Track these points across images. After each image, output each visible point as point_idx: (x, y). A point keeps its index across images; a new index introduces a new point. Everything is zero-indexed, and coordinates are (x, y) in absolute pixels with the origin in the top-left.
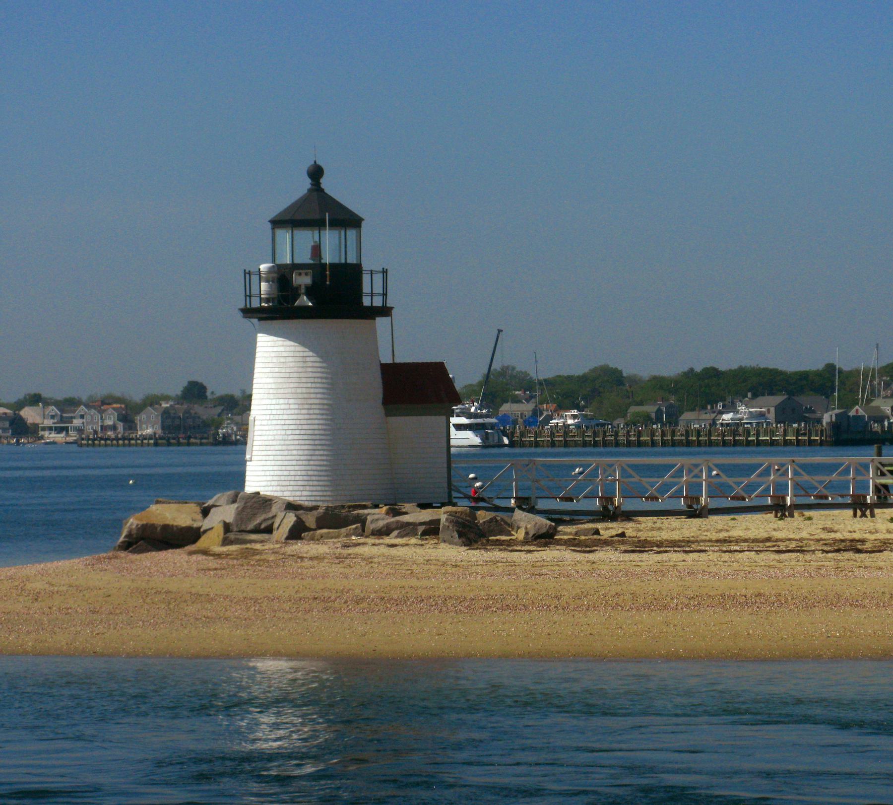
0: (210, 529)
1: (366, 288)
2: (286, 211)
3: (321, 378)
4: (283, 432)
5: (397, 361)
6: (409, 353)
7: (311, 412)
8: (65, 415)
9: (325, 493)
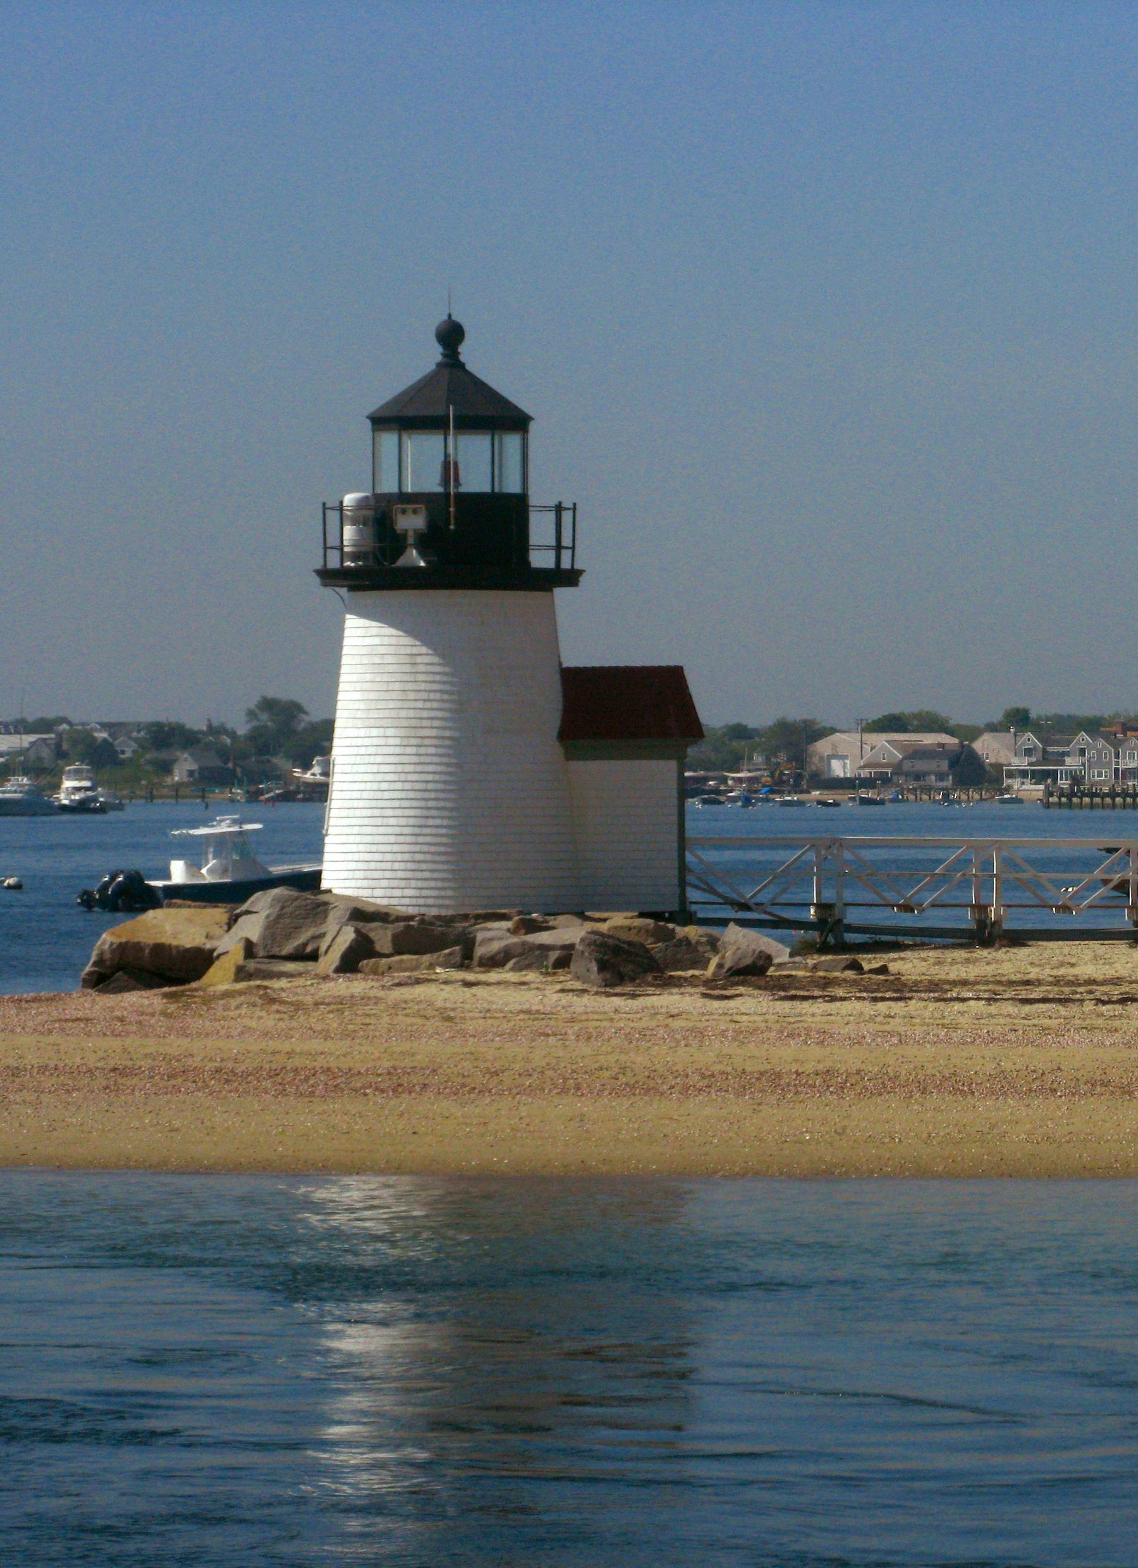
0: (224, 954)
1: (534, 538)
2: (397, 400)
3: (441, 691)
4: (375, 786)
7: (422, 750)
8: (1050, 749)
9: (443, 893)
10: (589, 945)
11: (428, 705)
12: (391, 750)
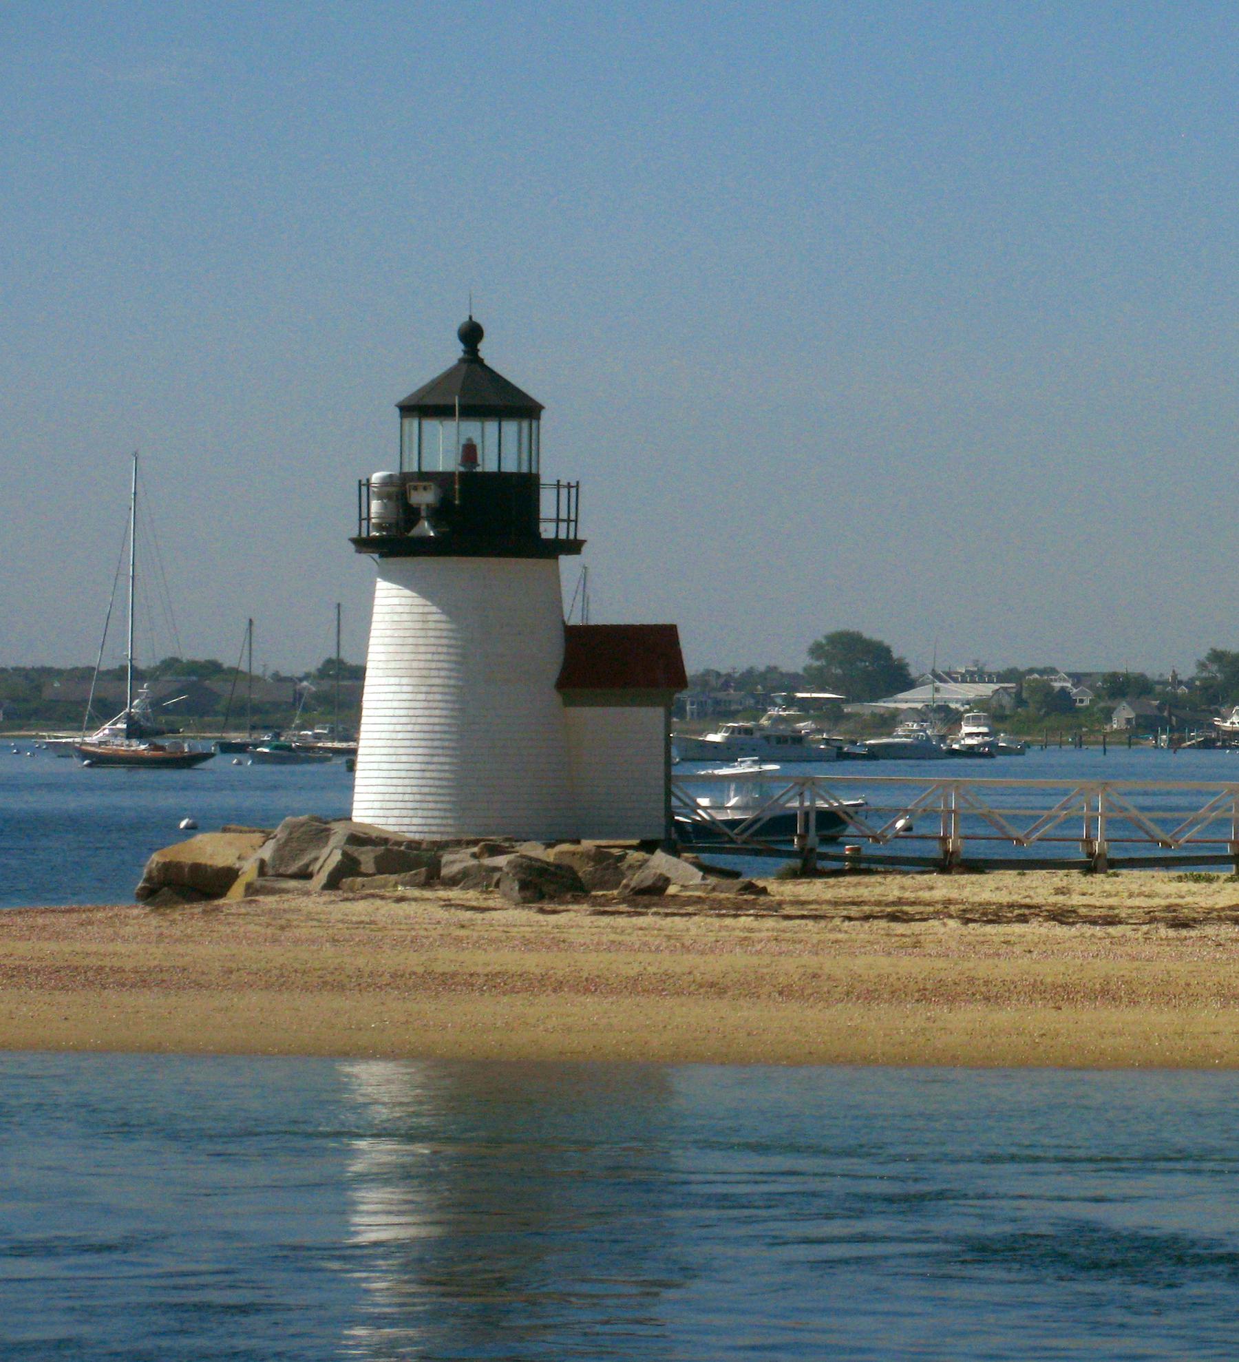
4: (391, 728)
5: (592, 622)
6: (611, 609)
7: (431, 697)
10: (515, 867)
11: (436, 657)
12: (405, 696)
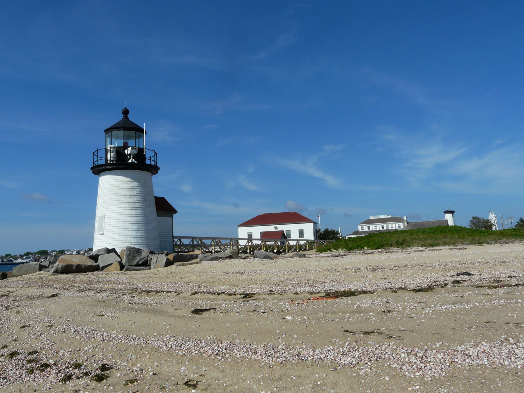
4: (123, 220)
